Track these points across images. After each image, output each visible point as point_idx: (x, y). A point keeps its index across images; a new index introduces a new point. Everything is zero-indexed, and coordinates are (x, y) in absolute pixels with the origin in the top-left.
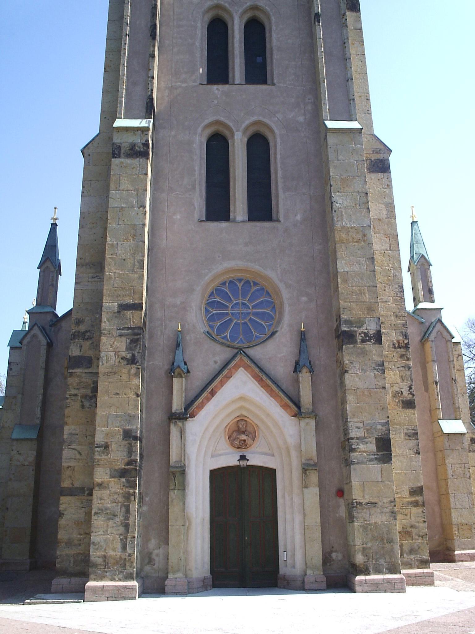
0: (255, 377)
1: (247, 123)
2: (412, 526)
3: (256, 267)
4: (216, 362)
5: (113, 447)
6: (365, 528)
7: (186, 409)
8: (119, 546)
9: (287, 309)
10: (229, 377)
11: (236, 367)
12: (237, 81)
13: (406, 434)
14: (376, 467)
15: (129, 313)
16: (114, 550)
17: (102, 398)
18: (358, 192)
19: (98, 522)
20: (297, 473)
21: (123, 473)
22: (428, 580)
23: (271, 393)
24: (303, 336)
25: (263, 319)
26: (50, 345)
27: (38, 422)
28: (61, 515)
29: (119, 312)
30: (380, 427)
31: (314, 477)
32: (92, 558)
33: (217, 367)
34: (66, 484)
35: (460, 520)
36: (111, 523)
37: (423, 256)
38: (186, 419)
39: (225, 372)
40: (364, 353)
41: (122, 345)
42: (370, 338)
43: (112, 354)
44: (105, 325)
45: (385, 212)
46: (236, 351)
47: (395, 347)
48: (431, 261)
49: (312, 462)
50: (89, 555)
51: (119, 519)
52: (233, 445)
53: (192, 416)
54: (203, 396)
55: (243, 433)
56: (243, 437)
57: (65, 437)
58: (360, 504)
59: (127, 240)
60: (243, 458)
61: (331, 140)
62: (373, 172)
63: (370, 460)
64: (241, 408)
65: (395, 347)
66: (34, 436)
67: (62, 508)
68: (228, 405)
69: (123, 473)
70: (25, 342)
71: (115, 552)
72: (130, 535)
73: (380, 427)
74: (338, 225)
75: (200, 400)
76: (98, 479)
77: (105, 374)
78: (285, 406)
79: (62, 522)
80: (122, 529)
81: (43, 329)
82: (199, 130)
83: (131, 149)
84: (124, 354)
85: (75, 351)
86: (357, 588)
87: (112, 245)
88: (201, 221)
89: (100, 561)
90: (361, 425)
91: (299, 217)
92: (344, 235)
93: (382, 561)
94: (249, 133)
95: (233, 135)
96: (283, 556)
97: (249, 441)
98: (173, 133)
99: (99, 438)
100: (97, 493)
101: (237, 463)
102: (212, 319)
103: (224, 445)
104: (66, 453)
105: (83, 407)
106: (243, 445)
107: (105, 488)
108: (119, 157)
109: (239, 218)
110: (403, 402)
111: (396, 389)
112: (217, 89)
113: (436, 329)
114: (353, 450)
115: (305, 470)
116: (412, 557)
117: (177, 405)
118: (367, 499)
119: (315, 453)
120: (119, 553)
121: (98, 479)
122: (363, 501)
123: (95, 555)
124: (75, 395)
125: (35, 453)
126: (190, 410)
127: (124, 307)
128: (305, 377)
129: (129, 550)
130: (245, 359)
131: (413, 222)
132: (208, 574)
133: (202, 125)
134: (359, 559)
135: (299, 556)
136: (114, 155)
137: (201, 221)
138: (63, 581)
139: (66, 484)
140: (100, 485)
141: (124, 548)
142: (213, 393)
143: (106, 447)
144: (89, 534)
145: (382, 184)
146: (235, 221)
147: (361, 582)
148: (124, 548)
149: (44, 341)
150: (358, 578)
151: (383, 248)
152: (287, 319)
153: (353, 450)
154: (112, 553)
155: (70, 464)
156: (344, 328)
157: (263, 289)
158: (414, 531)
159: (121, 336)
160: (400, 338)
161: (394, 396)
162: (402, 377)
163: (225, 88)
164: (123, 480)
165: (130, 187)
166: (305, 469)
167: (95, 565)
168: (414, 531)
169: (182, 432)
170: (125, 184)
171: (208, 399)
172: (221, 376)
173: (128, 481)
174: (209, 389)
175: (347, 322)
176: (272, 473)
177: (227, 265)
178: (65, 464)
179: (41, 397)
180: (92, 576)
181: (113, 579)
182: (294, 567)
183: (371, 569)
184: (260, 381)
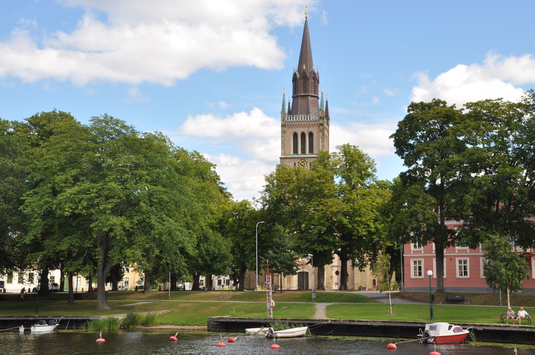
67: (201, 155)
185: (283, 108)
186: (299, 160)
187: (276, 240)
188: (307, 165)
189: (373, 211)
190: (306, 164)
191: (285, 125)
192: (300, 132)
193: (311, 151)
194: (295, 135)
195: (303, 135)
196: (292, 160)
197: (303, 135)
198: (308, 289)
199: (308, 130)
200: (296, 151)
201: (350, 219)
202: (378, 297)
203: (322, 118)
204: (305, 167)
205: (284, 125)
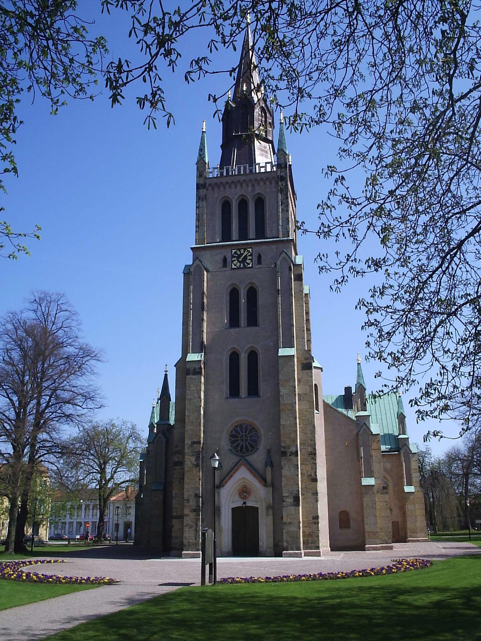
0: (249, 470)
1: (247, 348)
2: (313, 532)
3: (250, 420)
4: (233, 463)
5: (191, 500)
6: (287, 532)
7: (220, 483)
8: (194, 538)
9: (263, 439)
10: (237, 470)
11: (241, 465)
12: (242, 326)
13: (312, 493)
14: (293, 508)
15: (195, 445)
16: (192, 540)
17: (186, 480)
18: (291, 386)
19: (186, 529)
20: (264, 510)
21: (195, 511)
22: (318, 554)
23: (254, 476)
24: (269, 451)
25: (251, 447)
26: (167, 442)
27: (163, 481)
28: (173, 526)
29: (191, 445)
30: (295, 492)
31: (271, 512)
32: (185, 543)
33: (233, 465)
34: (174, 514)
35: (370, 530)
36: (191, 529)
37: (361, 384)
38: (220, 488)
39: (236, 467)
40: (290, 460)
41: (193, 459)
42: (293, 454)
43: (189, 463)
44: (186, 450)
45: (308, 390)
46: (240, 458)
47: (309, 455)
48: (366, 388)
49: (270, 505)
50: (183, 542)
51: (193, 528)
52: (241, 498)
53: (223, 486)
54: (227, 478)
55: (245, 492)
56: (245, 494)
57: (173, 495)
58: (286, 523)
59: (193, 413)
60: (245, 503)
61: (280, 361)
62: (304, 370)
63: (291, 505)
64: (244, 482)
65: (309, 455)
66: (162, 488)
67: (173, 523)
68: (237, 481)
69: (195, 511)
70: (155, 441)
71: (193, 541)
72: (198, 534)
73: (295, 492)
74: (282, 402)
75: (226, 480)
76: (186, 512)
77: (187, 471)
78: (260, 482)
79: (173, 529)
80: (195, 532)
81: (164, 434)
82: (225, 353)
83: (194, 371)
84: (194, 463)
85: (176, 459)
86: (283, 556)
87: (188, 416)
88: (227, 398)
89: (187, 544)
90: (287, 491)
91: (269, 395)
92: (284, 407)
93: (294, 546)
94: (248, 352)
95: (241, 354)
96: (261, 544)
97: (247, 496)
98: (214, 355)
99: (186, 496)
100: (185, 518)
101: (241, 505)
102: (232, 443)
103: (237, 498)
104: (174, 502)
105: (180, 482)
106: (245, 497)
107: (189, 516)
108: (189, 375)
109: (243, 396)
110: (312, 479)
111: (309, 473)
112: (233, 331)
113: (363, 429)
114: (284, 501)
115: (267, 509)
116: (313, 545)
117: (217, 482)
118: (289, 521)
119: (272, 502)
120: (194, 541)
121: (186, 512)
122: (287, 522)
123: (185, 542)
124: (177, 478)
125: (163, 496)
126: (222, 484)
127: (194, 443)
128: (269, 469)
129: (197, 540)
130: (245, 462)
131: (358, 364)
132: (231, 550)
133: (227, 350)
134: (285, 544)
135: (265, 543)
136: (188, 374)
137: (227, 398)
138: (175, 552)
139: (174, 514)
140: (186, 515)
141: (196, 539)
142: (231, 477)
143: (188, 500)
144: (183, 534)
145: (308, 376)
146: (241, 398)
147: (284, 553)
148: (196, 539)
149: (164, 440)
150: (284, 552)
151: (307, 408)
152: (263, 443)
153: (284, 501)
154: (192, 541)
155: (176, 506)
156: (282, 450)
157: (253, 428)
158: (314, 534)
159: (192, 455)
160: (312, 450)
161: (308, 476)
162: (312, 468)
163: (237, 330)
164: (195, 513)
165: (195, 389)
166: (267, 509)
167: (185, 546)
168: (314, 534)
169: (219, 493)
170: (193, 388)
171: (229, 479)
172: (234, 469)
173: (197, 514)
174: (229, 475)
175: (284, 447)
176: (257, 509)
177: (238, 418)
178: (174, 506)
179: (164, 468)
180: (185, 549)
181: (192, 551)
182: (263, 548)
183: (289, 548)
184: (250, 471)
185: (201, 153)
186: (233, 251)
187: (145, 452)
188: (251, 260)
189: (452, 223)
190: (251, 258)
191: (205, 184)
192: (237, 196)
193: (260, 233)
194: (226, 206)
195: (243, 204)
196: (218, 251)
197: (243, 204)
198: (264, 236)
199: (253, 190)
200: (226, 236)
201: (421, 174)
202: (429, 588)
203: (283, 166)
204: (249, 264)
205: (202, 185)
